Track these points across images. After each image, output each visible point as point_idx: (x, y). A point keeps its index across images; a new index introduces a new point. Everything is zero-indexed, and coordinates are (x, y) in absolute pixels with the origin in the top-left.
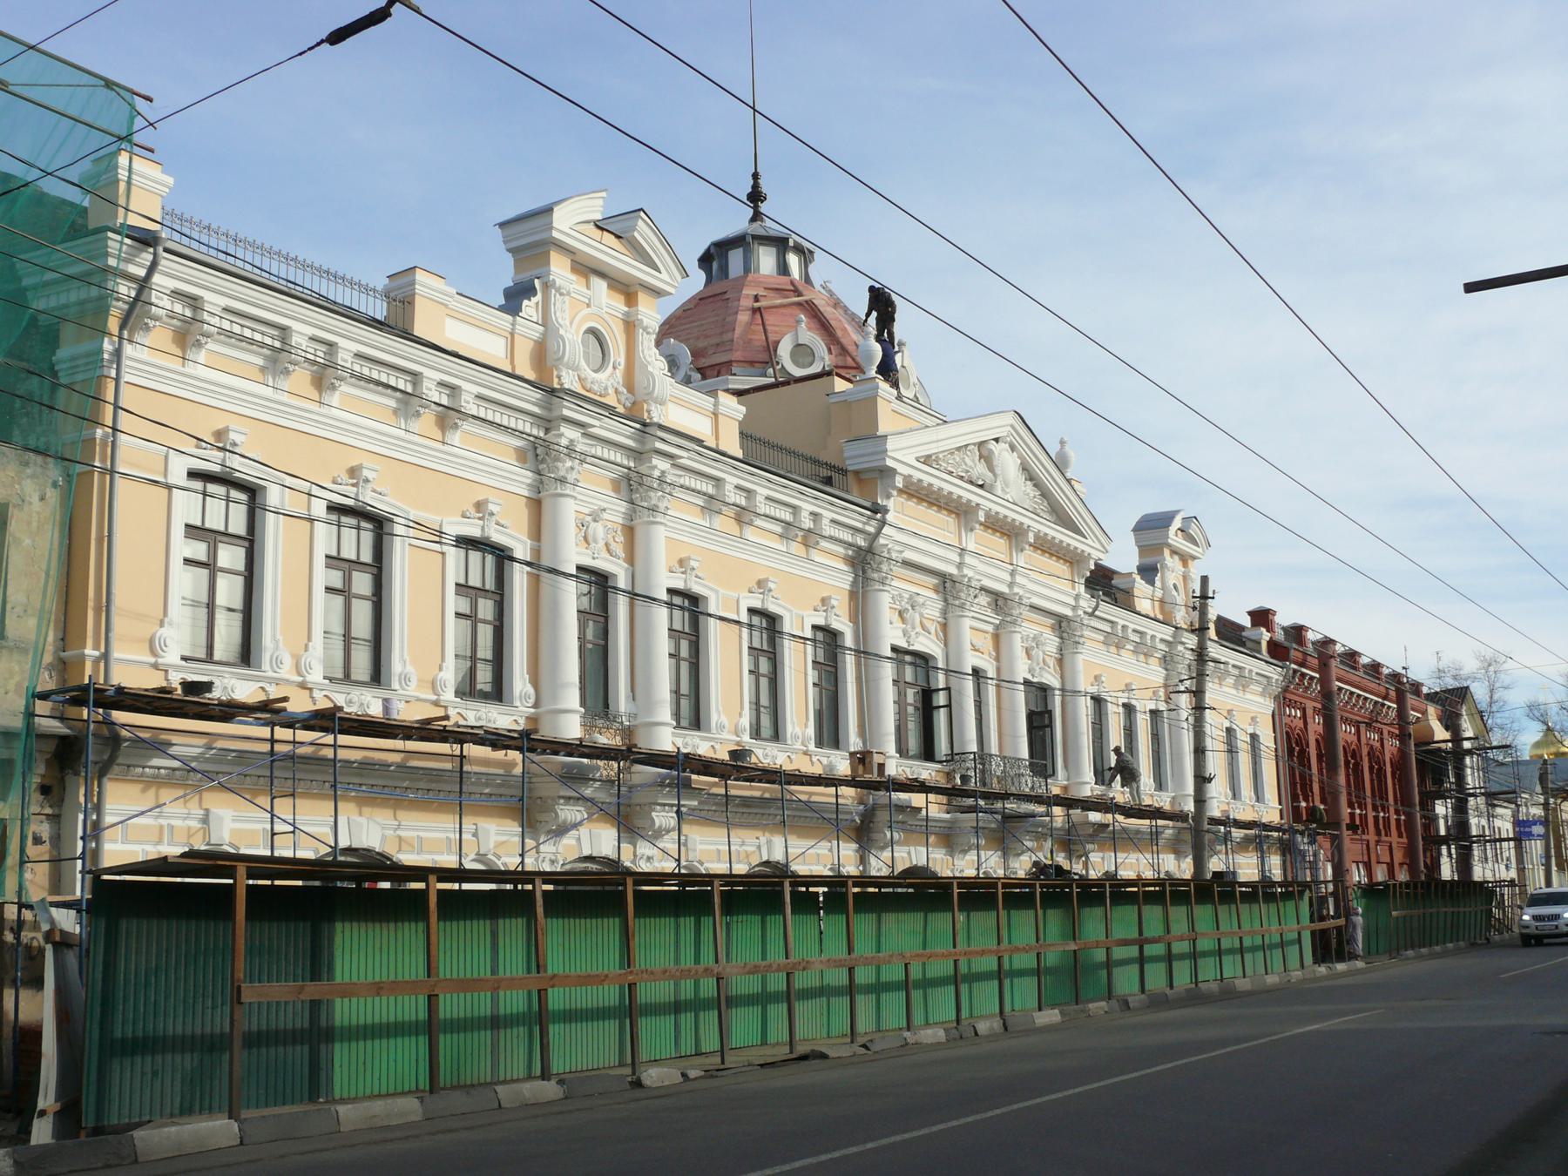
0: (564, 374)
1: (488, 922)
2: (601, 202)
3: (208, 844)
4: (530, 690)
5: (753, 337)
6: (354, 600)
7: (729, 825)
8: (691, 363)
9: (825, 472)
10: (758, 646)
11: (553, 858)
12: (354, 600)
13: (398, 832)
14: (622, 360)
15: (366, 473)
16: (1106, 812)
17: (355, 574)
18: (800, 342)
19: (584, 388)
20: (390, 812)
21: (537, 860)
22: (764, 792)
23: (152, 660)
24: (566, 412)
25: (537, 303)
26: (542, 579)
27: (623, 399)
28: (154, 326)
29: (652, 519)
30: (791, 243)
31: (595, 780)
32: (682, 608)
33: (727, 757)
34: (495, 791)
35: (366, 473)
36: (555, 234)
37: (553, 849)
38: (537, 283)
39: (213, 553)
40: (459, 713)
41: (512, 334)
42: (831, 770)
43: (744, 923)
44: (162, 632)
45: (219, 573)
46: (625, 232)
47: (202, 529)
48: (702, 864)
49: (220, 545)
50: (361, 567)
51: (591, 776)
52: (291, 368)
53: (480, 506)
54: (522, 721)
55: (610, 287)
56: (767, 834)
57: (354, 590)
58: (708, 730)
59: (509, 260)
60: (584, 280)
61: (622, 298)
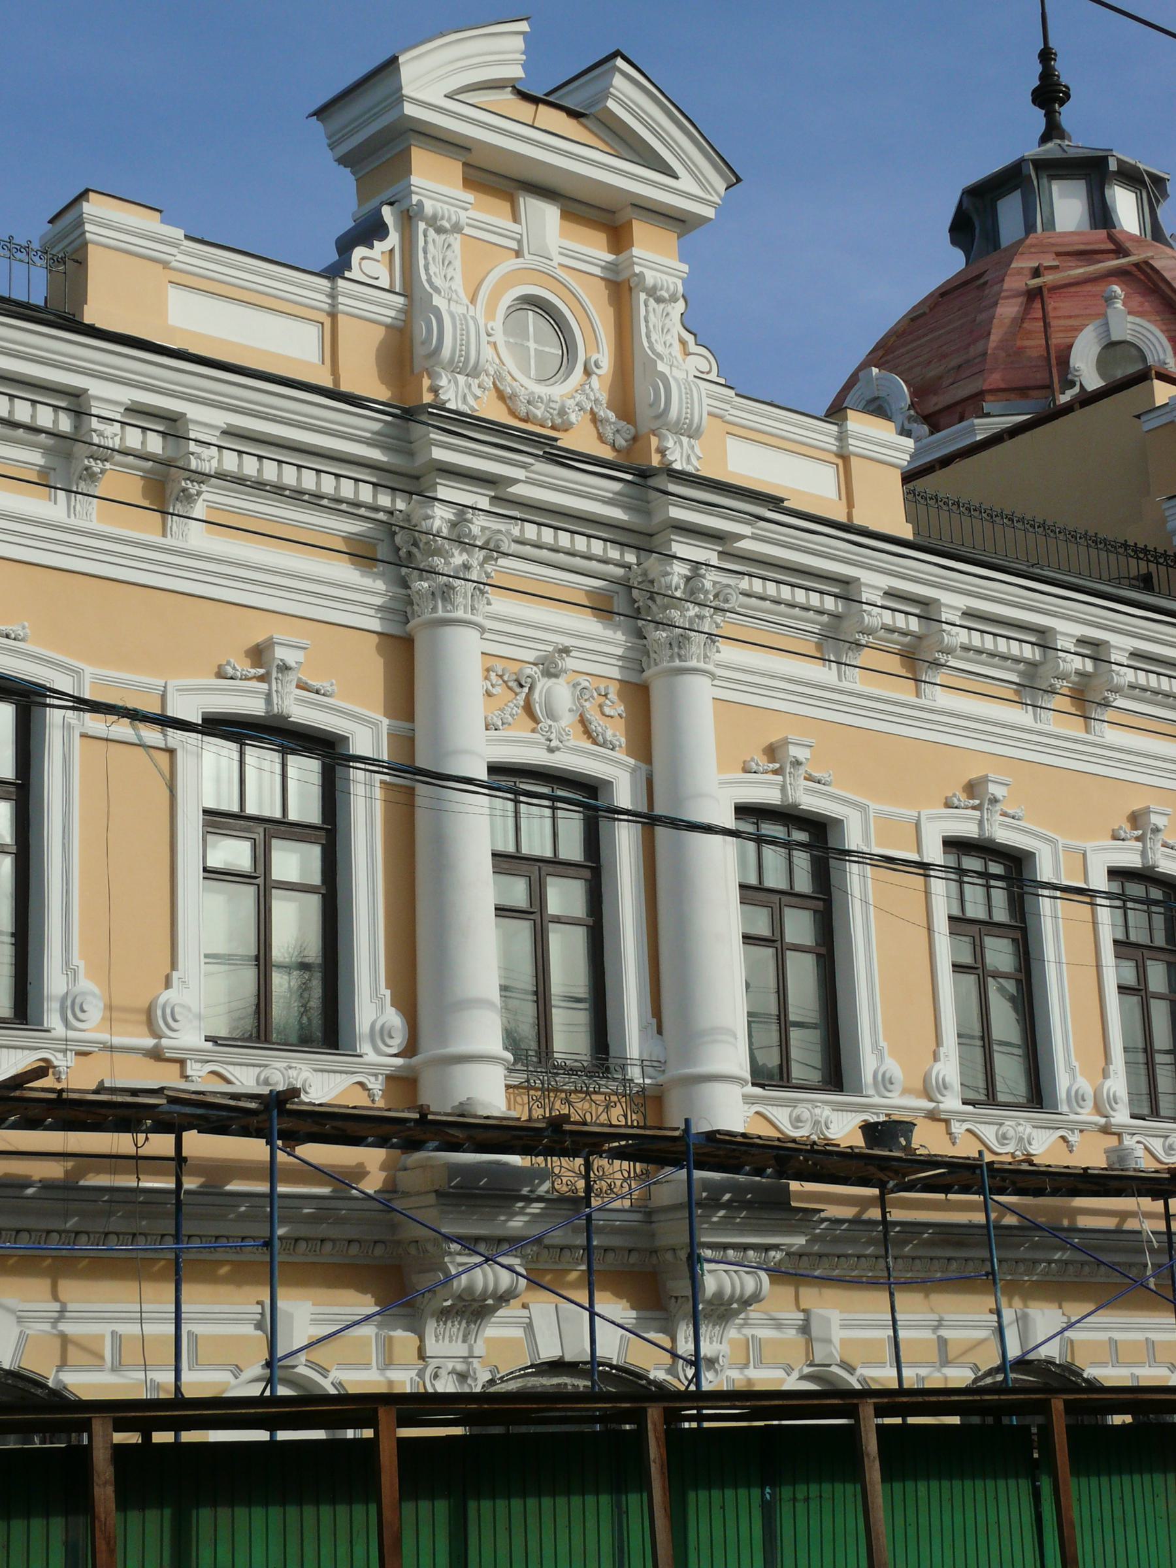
0: (443, 382)
1: (605, 1499)
2: (519, 43)
3: (811, 1365)
4: (394, 1019)
5: (1027, 343)
6: (788, 953)
7: (890, 1285)
8: (912, 406)
9: (1138, 567)
10: (1143, 939)
11: (460, 1367)
12: (788, 953)
13: (64, 1327)
14: (605, 359)
15: (280, 653)
16: (537, 1155)
17: (989, 941)
18: (1115, 337)
19: (513, 413)
20: (44, 1285)
21: (421, 1374)
22: (864, 1210)
23: (149, 1042)
24: (438, 454)
25: (392, 251)
26: (419, 801)
27: (609, 432)
28: (103, 472)
29: (677, 663)
30: (1113, 166)
31: (528, 1200)
32: (802, 845)
33: (859, 1141)
34: (304, 1231)
35: (280, 653)
36: (409, 110)
37: (461, 1349)
38: (387, 213)
39: (263, 858)
40: (968, 1130)
41: (333, 315)
42: (1122, 1159)
43: (814, 1505)
44: (166, 996)
45: (274, 891)
46: (591, 105)
47: (760, 889)
48: (324, 1372)
49: (549, 879)
50: (996, 930)
51: (525, 1191)
52: (97, 467)
53: (259, 654)
54: (376, 1085)
55: (566, 215)
56: (1017, 1302)
57: (789, 938)
58: (858, 1090)
59: (346, 179)
60: (506, 206)
61: (601, 238)
